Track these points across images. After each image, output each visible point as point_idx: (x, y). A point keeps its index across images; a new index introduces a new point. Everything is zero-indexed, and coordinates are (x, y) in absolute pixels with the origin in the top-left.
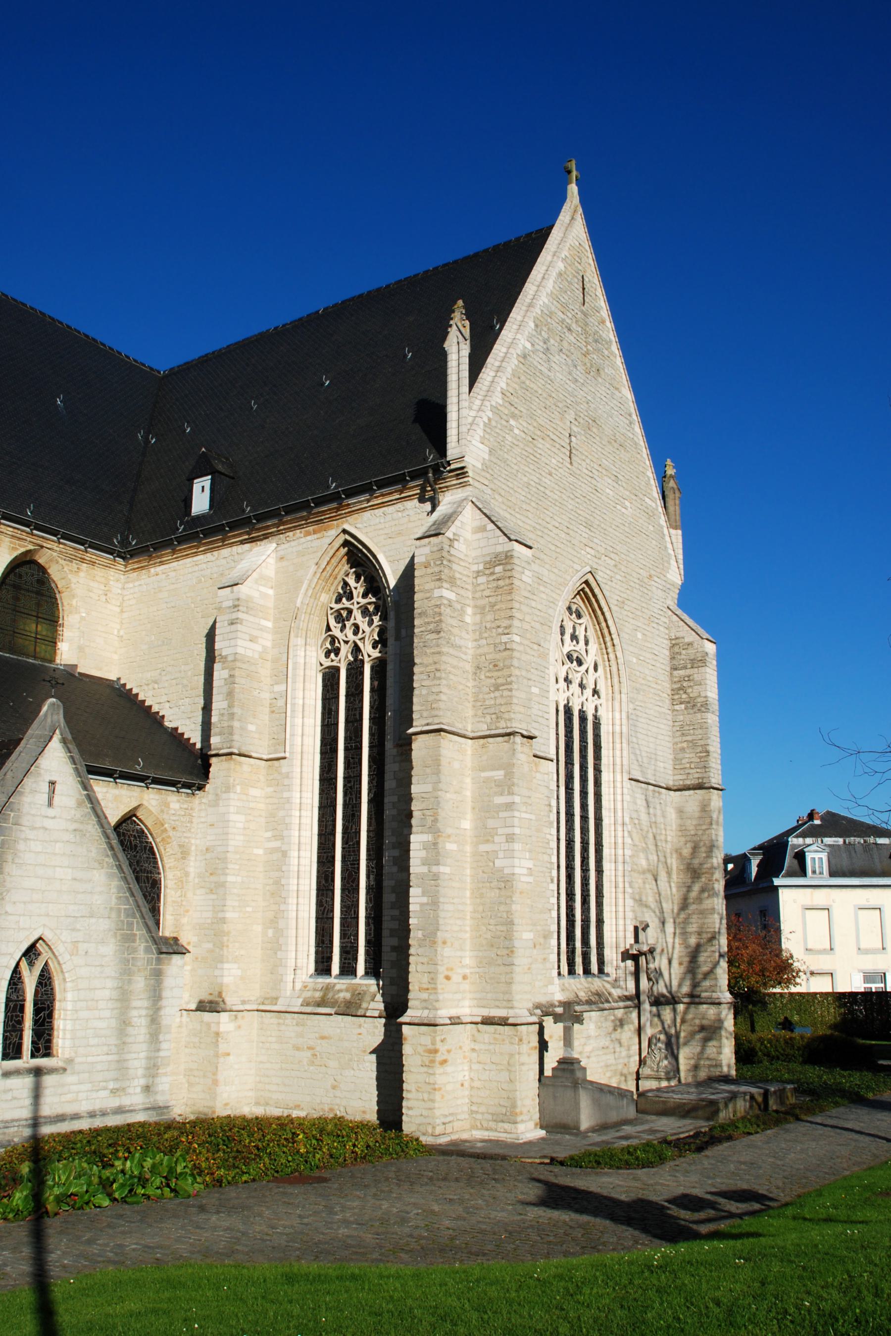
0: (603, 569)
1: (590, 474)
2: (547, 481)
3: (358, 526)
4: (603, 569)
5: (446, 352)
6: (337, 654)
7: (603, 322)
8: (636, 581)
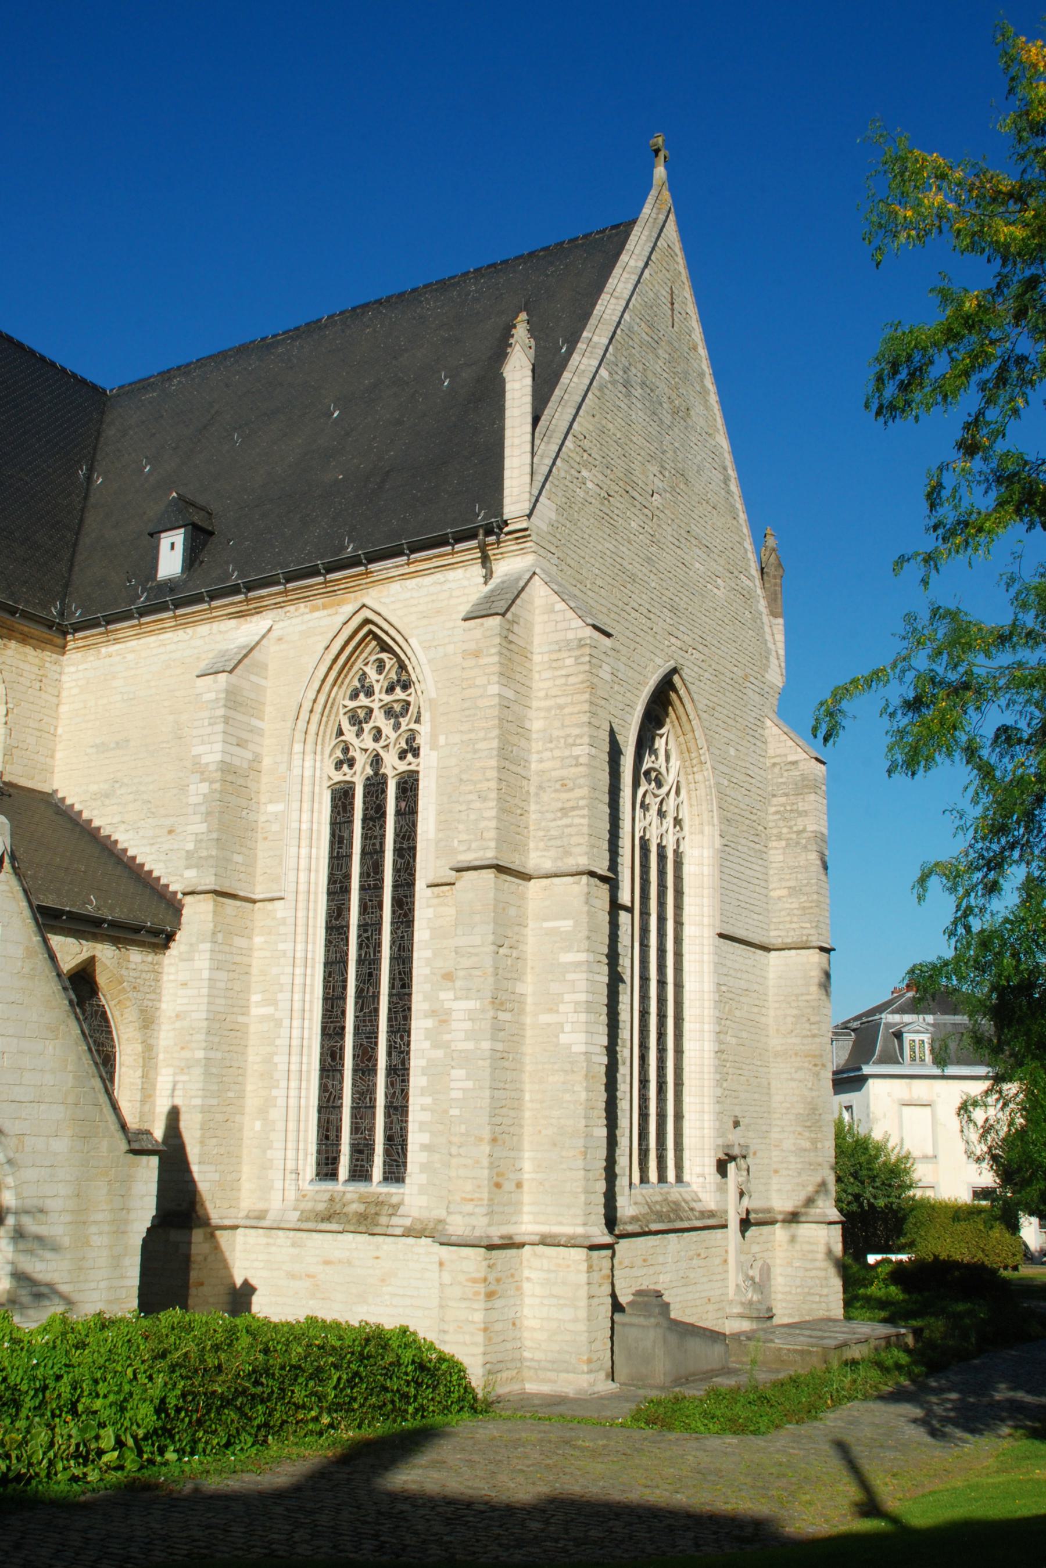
0: (691, 665)
1: (677, 543)
2: (624, 549)
3: (383, 600)
4: (691, 665)
5: (504, 379)
6: (351, 766)
7: (695, 349)
8: (728, 681)
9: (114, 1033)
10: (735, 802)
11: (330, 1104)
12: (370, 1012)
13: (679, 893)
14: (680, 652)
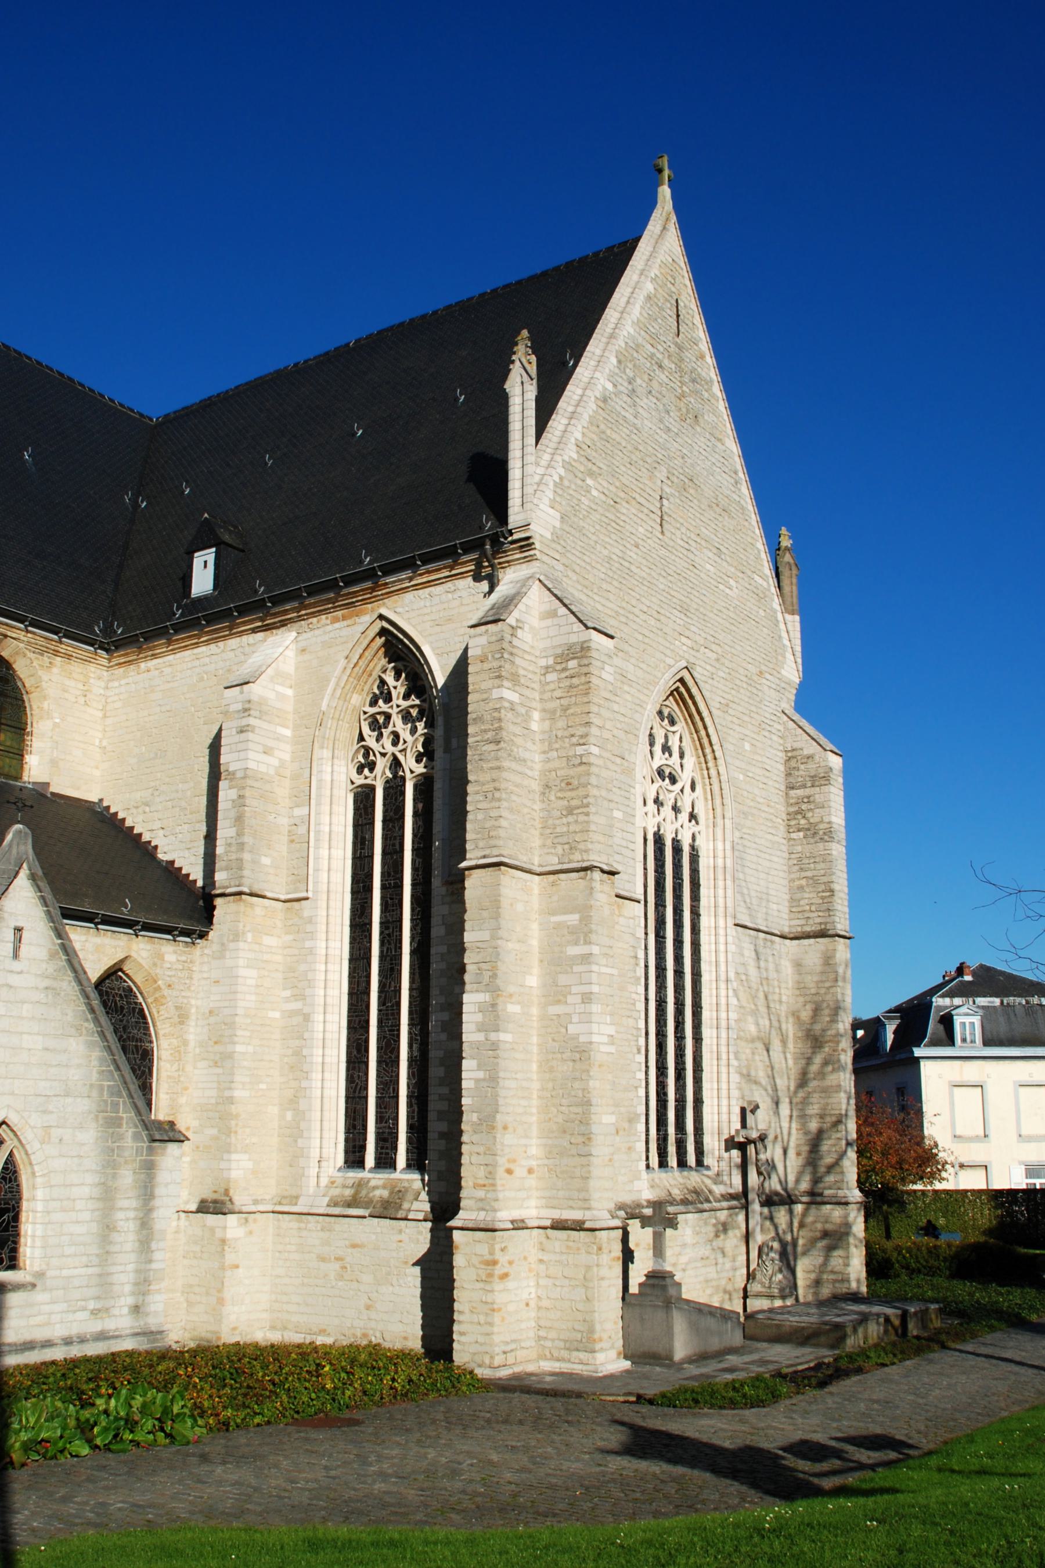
0: (703, 664)
3: (398, 610)
4: (703, 664)
6: (371, 770)
9: (152, 1029)
10: (750, 796)
11: (357, 1094)
12: (392, 1006)
13: (695, 885)
14: (691, 651)
